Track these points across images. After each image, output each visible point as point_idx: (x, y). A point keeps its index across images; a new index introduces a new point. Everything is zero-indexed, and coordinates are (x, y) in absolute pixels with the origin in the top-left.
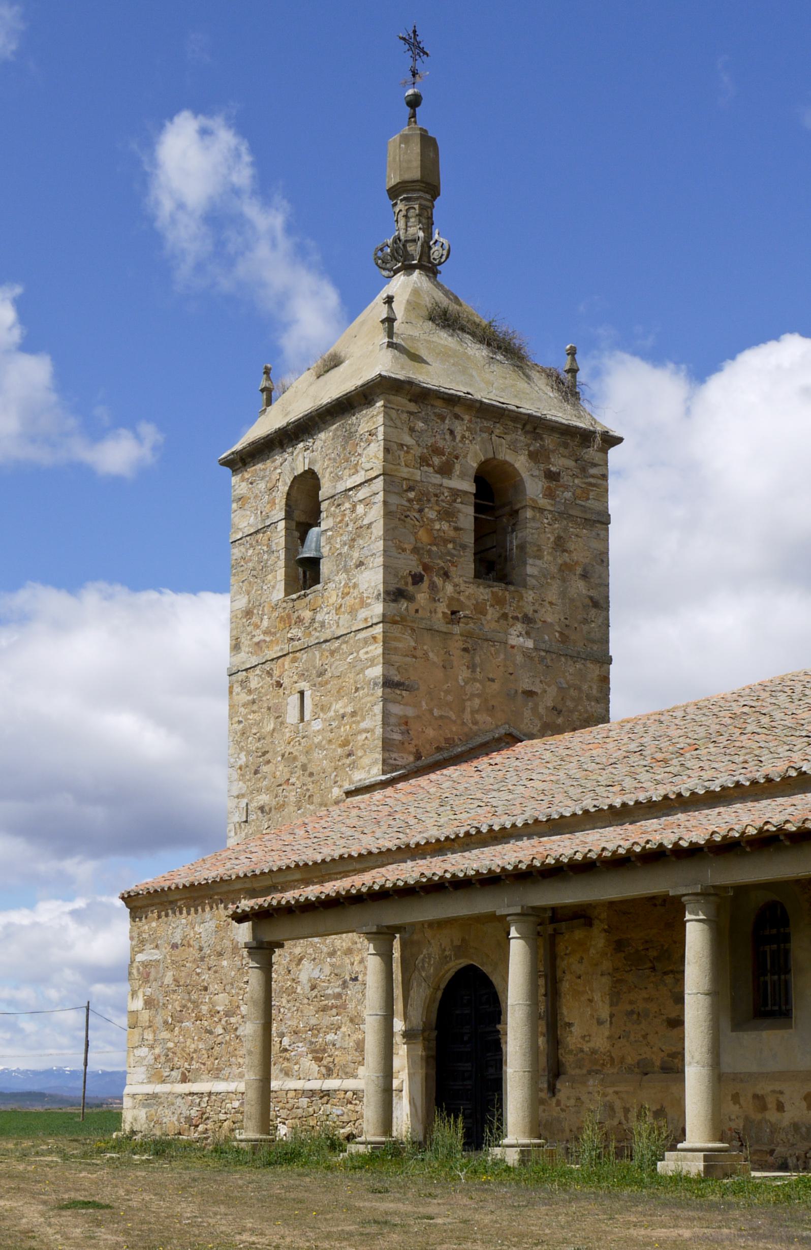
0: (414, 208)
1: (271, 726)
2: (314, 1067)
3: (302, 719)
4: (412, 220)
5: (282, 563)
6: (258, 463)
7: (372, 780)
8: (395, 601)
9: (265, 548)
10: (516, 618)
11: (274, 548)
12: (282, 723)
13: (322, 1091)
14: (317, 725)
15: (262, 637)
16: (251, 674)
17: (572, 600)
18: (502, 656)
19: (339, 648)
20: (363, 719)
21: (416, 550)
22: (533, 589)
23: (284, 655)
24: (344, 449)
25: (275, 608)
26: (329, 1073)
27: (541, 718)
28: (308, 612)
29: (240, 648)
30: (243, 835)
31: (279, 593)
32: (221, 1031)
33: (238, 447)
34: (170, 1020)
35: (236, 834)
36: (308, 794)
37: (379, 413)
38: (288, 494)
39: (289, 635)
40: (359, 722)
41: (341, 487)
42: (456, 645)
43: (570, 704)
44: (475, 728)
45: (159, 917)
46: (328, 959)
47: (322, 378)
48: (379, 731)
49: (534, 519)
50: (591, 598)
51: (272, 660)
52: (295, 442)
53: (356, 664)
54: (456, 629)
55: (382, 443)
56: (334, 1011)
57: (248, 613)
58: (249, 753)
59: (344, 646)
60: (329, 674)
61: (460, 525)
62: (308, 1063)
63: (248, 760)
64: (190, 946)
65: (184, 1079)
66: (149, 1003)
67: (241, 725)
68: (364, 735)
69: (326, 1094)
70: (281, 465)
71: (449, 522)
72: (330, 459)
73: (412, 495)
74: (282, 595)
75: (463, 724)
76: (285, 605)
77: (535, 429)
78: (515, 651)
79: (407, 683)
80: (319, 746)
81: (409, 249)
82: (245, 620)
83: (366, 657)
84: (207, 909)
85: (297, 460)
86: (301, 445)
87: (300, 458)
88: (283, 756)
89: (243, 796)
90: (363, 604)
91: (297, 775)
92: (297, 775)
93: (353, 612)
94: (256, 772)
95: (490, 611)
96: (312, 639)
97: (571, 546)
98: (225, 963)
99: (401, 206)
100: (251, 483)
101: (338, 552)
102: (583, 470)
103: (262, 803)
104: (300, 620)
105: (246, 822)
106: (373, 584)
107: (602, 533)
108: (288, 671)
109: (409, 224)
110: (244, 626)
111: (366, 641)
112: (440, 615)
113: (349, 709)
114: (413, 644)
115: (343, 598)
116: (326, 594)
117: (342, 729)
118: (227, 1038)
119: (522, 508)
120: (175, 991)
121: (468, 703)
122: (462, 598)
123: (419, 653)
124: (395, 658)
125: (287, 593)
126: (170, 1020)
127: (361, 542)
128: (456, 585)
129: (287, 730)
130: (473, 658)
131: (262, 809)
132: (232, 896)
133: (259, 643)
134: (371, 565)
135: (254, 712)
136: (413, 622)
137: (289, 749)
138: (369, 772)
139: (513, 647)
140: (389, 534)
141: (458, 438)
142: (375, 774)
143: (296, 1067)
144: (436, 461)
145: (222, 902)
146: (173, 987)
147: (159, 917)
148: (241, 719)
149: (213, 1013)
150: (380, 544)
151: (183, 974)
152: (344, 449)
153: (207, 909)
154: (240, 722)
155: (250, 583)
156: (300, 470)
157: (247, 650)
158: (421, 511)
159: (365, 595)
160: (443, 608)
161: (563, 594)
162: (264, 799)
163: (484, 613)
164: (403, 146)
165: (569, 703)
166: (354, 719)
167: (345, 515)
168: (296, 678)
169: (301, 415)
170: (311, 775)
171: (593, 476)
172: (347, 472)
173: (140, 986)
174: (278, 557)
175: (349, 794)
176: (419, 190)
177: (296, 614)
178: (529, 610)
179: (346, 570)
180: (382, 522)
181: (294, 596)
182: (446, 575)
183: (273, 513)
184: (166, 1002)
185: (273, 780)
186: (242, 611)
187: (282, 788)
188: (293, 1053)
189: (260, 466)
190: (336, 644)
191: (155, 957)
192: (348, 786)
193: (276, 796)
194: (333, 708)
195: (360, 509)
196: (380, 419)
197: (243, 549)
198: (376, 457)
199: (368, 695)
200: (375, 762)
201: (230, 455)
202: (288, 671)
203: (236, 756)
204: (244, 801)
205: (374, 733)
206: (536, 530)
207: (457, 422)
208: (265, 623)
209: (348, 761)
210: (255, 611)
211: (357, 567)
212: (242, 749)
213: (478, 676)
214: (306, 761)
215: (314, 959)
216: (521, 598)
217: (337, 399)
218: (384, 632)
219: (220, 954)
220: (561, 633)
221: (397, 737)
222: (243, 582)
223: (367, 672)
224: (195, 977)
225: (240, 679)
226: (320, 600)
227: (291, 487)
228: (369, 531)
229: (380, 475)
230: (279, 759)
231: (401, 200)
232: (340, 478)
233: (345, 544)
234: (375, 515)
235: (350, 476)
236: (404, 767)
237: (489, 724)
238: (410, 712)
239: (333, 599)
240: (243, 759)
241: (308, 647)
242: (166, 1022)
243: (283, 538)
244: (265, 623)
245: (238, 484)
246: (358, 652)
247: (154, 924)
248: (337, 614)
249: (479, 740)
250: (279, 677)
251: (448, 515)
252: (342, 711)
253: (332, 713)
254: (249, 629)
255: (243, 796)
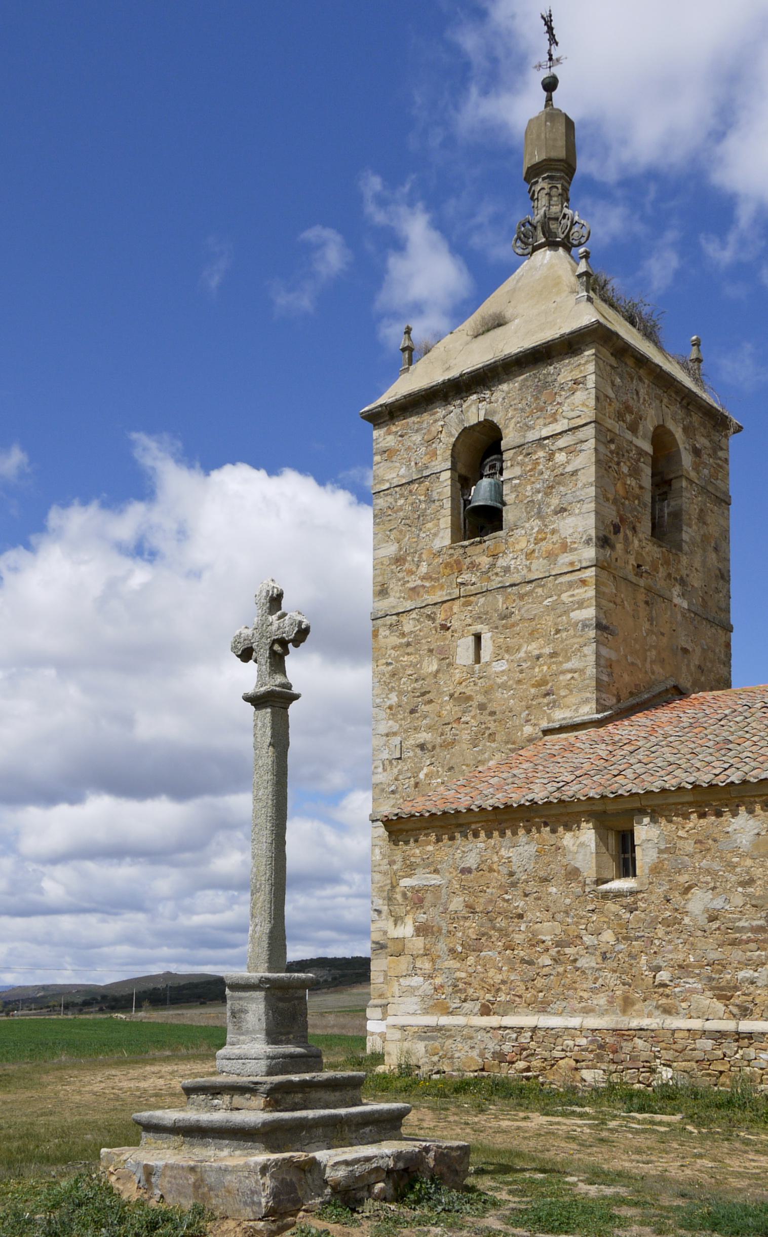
0: (557, 188)
1: (435, 667)
2: (719, 1006)
3: (478, 659)
4: (555, 199)
5: (448, 511)
6: (411, 416)
7: (585, 718)
8: (603, 547)
9: (422, 498)
10: (675, 579)
11: (435, 496)
12: (450, 665)
13: (738, 1033)
14: (499, 666)
15: (419, 582)
16: (404, 619)
17: (709, 569)
18: (669, 613)
19: (531, 592)
20: (568, 659)
21: (615, 501)
22: (686, 554)
23: (453, 599)
24: (537, 398)
25: (439, 553)
26: (745, 1012)
27: (692, 675)
28: (485, 557)
29: (387, 593)
30: (395, 771)
31: (444, 539)
32: (548, 962)
33: (382, 400)
34: (460, 949)
35: (385, 770)
36: (488, 732)
37: (587, 362)
38: (454, 445)
39: (459, 580)
40: (561, 663)
41: (532, 436)
42: (641, 597)
43: (709, 665)
44: (653, 677)
45: (439, 840)
46: (740, 889)
47: (480, 338)
48: (591, 671)
49: (687, 488)
50: (720, 570)
51: (435, 604)
52: (464, 394)
53: (556, 607)
54: (642, 582)
55: (593, 391)
56: (753, 946)
57: (399, 560)
58: (401, 693)
59: (539, 590)
60: (516, 617)
61: (643, 485)
62: (706, 1001)
63: (400, 700)
64: (491, 870)
65: (486, 1011)
66: (422, 930)
67: (390, 668)
68: (569, 676)
69: (738, 1036)
70: (444, 417)
71: (635, 479)
72: (515, 409)
73: (613, 447)
74: (447, 541)
75: (646, 672)
76: (452, 551)
77: (688, 404)
78: (677, 609)
79: (611, 627)
80: (504, 686)
81: (552, 226)
82: (394, 567)
83: (571, 599)
84: (521, 832)
85: (472, 411)
86: (474, 397)
87: (473, 409)
88: (451, 696)
89: (395, 734)
90: (565, 547)
91: (472, 714)
92: (472, 714)
93: (551, 556)
94: (412, 711)
95: (661, 569)
96: (493, 583)
97: (709, 520)
98: (553, 890)
99: (542, 184)
100: (401, 436)
101: (529, 499)
102: (715, 452)
103: (422, 741)
104: (473, 566)
105: (400, 758)
106: (580, 529)
107: (726, 512)
108: (459, 616)
109: (552, 203)
110: (392, 572)
111: (571, 585)
112: (631, 567)
113: (547, 650)
114: (614, 591)
115: (536, 544)
116: (511, 540)
117: (537, 670)
118: (561, 970)
119: (676, 478)
120: (466, 918)
121: (648, 654)
122: (644, 553)
123: (618, 601)
124: (604, 602)
125: (453, 542)
126: (460, 949)
127: (562, 488)
128: (640, 541)
129: (457, 671)
130: (651, 611)
131: (422, 747)
132: (566, 819)
133: (415, 588)
134: (577, 511)
135: (408, 654)
136: (615, 569)
137: (460, 689)
138: (576, 710)
139: (675, 606)
140: (600, 483)
141: (641, 401)
142: (588, 711)
143: (684, 1005)
144: (628, 418)
145: (546, 824)
146: (464, 913)
147: (439, 840)
148: (390, 661)
149: (534, 942)
150: (592, 491)
151: (482, 900)
152: (537, 398)
153: (521, 832)
154: (388, 664)
155: (401, 531)
156: (473, 421)
157: (398, 595)
158: (618, 464)
159: (568, 540)
160: (632, 561)
161: (704, 563)
162: (424, 736)
163: (656, 570)
164: (548, 123)
165: (708, 664)
166: (554, 660)
167: (538, 464)
168: (469, 621)
169: (480, 365)
170: (493, 713)
171: (720, 459)
172: (541, 421)
173: (407, 913)
174: (442, 507)
175: (546, 732)
176: (562, 171)
177: (468, 560)
178: (684, 572)
179: (540, 515)
180: (593, 468)
181: (466, 543)
182: (634, 529)
183: (433, 463)
184: (452, 929)
185: (437, 719)
186: (390, 559)
187: (450, 726)
188: (677, 990)
189: (414, 419)
190: (528, 588)
191: (433, 882)
192: (545, 725)
193: (442, 734)
194: (524, 649)
195: (560, 457)
196: (591, 367)
197: (390, 499)
198: (583, 405)
199: (575, 636)
200: (587, 701)
201: (376, 408)
202: (459, 616)
203: (384, 696)
204: (396, 740)
205: (585, 673)
206: (689, 500)
207: (641, 384)
208: (424, 569)
209: (545, 701)
210: (409, 558)
211: (556, 513)
212: (392, 690)
213: (655, 630)
214: (485, 701)
215: (714, 889)
216: (679, 561)
217: (534, 348)
218: (596, 576)
219: (545, 880)
220: (702, 598)
221: (605, 678)
222: (390, 530)
223: (572, 615)
224: (501, 904)
225: (389, 623)
226: (503, 547)
227: (458, 438)
228: (574, 478)
229: (590, 423)
230: (447, 698)
231: (544, 179)
232: (530, 428)
233: (539, 492)
234: (584, 462)
235: (545, 425)
236: (611, 708)
237: (661, 675)
238: (614, 656)
239: (523, 544)
240: (394, 699)
241: (487, 591)
242: (452, 951)
243: (449, 488)
244: (424, 569)
245: (382, 437)
246: (559, 596)
247: (430, 848)
248: (528, 560)
249: (658, 689)
250: (446, 620)
251: (635, 472)
252: (537, 652)
253: (522, 654)
254: (400, 575)
255: (395, 734)
